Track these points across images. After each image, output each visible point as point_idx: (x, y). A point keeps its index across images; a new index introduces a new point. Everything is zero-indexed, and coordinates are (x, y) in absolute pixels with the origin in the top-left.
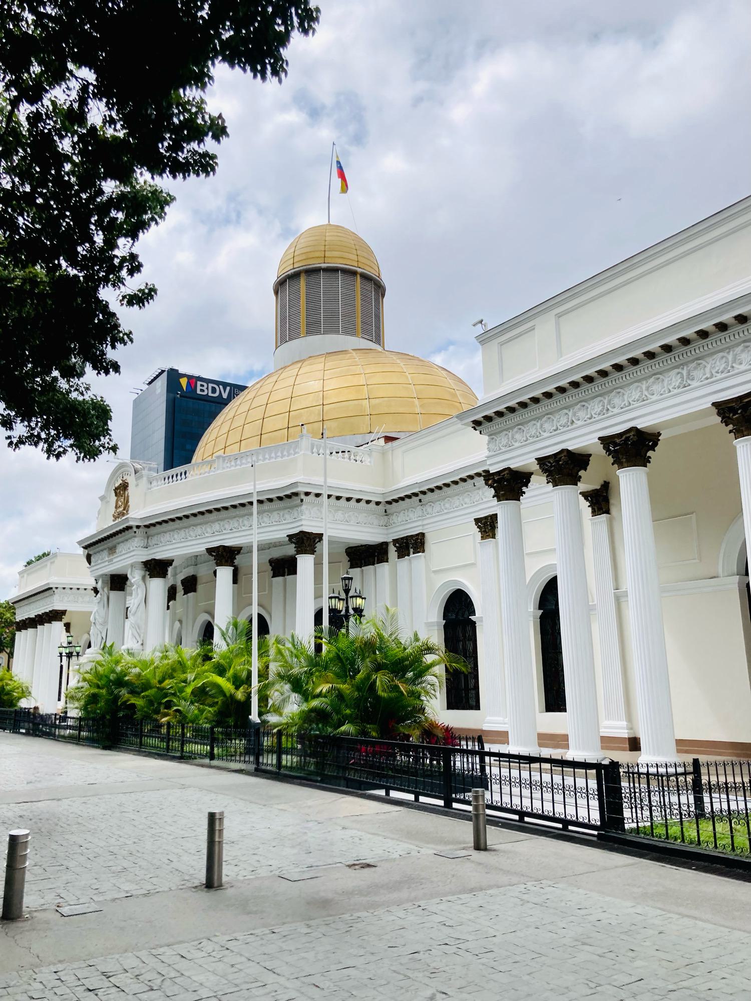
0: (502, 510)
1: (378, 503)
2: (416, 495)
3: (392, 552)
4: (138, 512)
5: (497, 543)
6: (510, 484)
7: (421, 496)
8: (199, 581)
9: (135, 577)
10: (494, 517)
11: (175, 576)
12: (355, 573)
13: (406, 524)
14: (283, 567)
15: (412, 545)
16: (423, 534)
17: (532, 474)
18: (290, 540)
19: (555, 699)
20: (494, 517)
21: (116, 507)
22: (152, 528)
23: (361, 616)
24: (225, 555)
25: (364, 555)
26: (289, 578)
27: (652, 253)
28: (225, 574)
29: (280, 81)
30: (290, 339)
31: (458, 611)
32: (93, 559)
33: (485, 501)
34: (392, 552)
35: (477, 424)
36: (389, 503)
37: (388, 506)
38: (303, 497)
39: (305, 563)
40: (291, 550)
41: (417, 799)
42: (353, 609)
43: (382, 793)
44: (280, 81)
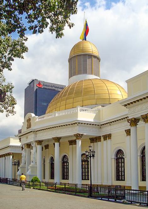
0: (133, 129)
1: (98, 125)
2: (109, 123)
3: (102, 138)
4: (33, 127)
5: (130, 137)
6: (134, 122)
7: (110, 123)
8: (49, 146)
9: (34, 145)
10: (130, 129)
11: (44, 144)
12: (92, 144)
13: (106, 130)
14: (72, 142)
15: (108, 137)
16: (111, 134)
17: (140, 119)
18: (75, 136)
19: (144, 179)
20: (130, 129)
21: (27, 125)
22: (38, 132)
23: (94, 157)
24: (58, 139)
25: (95, 140)
26: (74, 146)
27: (139, 113)
28: (57, 144)
29: (52, 33)
30: (73, 76)
31: (119, 156)
32: (21, 139)
33: (127, 126)
34: (102, 138)
35: (125, 105)
36: (101, 125)
37: (101, 126)
38: (78, 124)
39: (79, 143)
40: (74, 138)
41: (108, 199)
42: (92, 155)
43: (101, 198)
44: (52, 33)
